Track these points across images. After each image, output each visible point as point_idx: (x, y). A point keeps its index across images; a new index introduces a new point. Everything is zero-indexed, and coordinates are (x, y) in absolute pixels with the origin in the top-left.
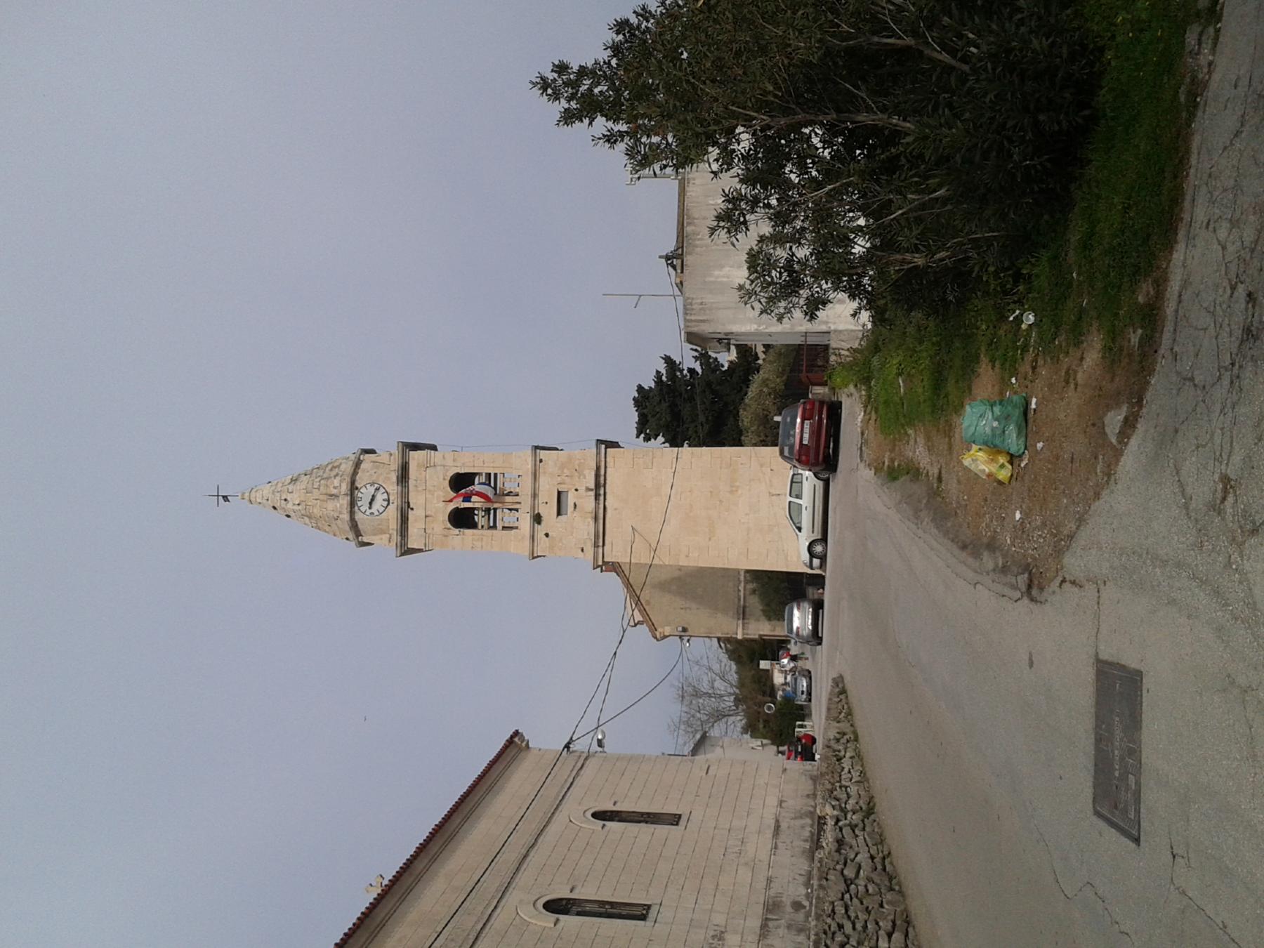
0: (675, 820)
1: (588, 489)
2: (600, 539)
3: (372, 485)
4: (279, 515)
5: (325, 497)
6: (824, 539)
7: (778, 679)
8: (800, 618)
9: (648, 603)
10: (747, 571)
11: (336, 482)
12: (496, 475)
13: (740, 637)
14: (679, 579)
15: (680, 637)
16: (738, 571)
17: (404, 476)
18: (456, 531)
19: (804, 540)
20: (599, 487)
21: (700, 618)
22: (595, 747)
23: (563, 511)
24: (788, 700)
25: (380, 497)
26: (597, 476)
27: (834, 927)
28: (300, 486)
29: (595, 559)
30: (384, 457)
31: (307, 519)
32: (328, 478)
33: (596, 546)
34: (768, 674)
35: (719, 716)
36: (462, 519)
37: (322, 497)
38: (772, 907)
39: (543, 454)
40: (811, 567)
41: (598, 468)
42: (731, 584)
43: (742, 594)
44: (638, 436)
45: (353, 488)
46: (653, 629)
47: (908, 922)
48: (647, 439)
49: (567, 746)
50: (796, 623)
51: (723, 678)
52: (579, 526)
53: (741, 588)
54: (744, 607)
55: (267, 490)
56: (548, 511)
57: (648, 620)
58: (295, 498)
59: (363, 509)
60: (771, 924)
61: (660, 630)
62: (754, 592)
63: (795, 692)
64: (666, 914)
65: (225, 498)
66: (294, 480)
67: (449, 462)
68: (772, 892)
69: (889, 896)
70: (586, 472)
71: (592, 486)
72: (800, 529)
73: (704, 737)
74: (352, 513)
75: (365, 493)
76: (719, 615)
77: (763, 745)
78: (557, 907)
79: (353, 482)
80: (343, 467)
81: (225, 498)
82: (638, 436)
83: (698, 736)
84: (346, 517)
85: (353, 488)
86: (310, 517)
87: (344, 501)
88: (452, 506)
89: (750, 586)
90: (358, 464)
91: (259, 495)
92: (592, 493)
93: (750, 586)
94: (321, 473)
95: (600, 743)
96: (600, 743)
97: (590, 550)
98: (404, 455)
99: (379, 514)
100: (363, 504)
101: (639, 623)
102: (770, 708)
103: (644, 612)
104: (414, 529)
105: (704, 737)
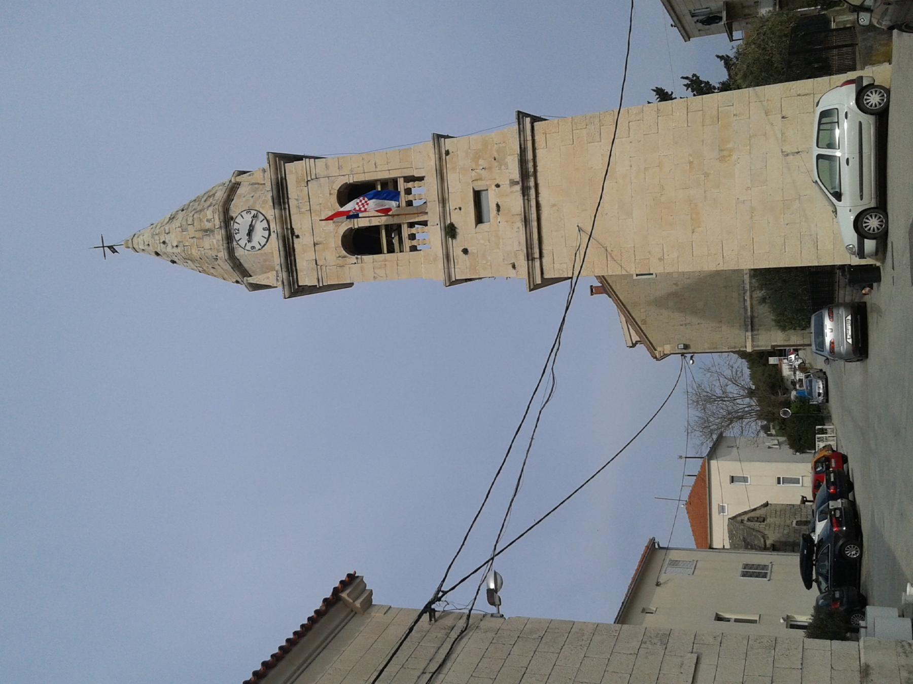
1: (513, 183)
2: (534, 250)
3: (248, 211)
4: (164, 263)
6: (881, 206)
7: (786, 371)
8: (835, 330)
9: (644, 322)
13: (749, 350)
14: (675, 294)
15: (683, 354)
16: (739, 272)
18: (353, 259)
19: (847, 218)
20: (527, 175)
21: (702, 332)
22: (483, 606)
23: (485, 218)
24: (804, 400)
25: (260, 226)
26: (523, 162)
28: (176, 223)
29: (530, 274)
30: (258, 177)
33: (530, 257)
34: (777, 368)
35: (734, 417)
36: (362, 242)
40: (861, 253)
41: (523, 151)
42: (735, 295)
43: (748, 303)
45: (227, 220)
46: (652, 348)
50: (829, 337)
51: (735, 383)
52: (504, 236)
53: (747, 297)
54: (752, 317)
55: (147, 237)
56: (464, 218)
58: (173, 239)
59: (242, 243)
61: (659, 349)
62: (763, 300)
63: (810, 393)
66: (172, 218)
67: (334, 171)
71: (516, 176)
72: (838, 196)
73: (721, 437)
75: (242, 223)
76: (724, 328)
77: (779, 444)
79: (226, 210)
83: (715, 437)
84: (223, 254)
87: (219, 235)
88: (345, 225)
89: (759, 294)
91: (140, 240)
92: (518, 188)
93: (759, 294)
95: (492, 595)
96: (492, 595)
97: (522, 263)
98: (277, 169)
99: (261, 247)
100: (241, 236)
101: (637, 342)
102: (785, 413)
103: (640, 331)
104: (303, 261)
105: (721, 437)
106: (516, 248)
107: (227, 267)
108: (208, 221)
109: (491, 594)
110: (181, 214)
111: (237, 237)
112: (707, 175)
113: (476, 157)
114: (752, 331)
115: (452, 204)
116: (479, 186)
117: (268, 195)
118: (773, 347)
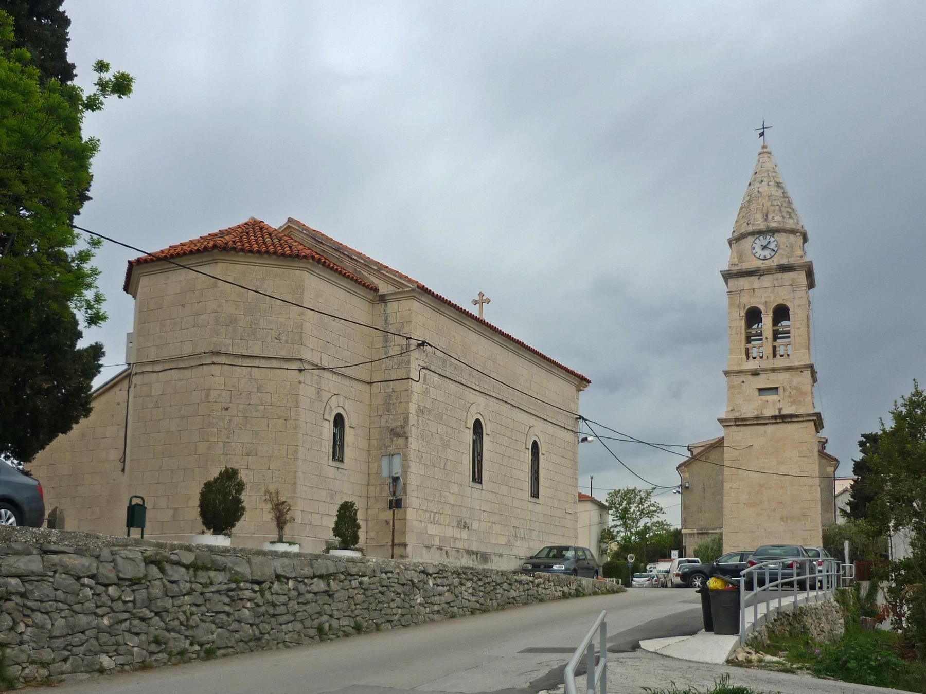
0: (535, 494)
1: (780, 410)
5: (765, 211)
10: (721, 534)
11: (778, 218)
12: (789, 337)
17: (784, 269)
18: (743, 313)
20: (783, 418)
22: (582, 436)
26: (791, 416)
27: (480, 577)
31: (748, 199)
32: (780, 211)
33: (736, 420)
36: (753, 316)
37: (765, 208)
38: (485, 557)
39: (808, 373)
41: (797, 416)
44: (863, 436)
45: (773, 231)
47: (484, 611)
48: (861, 444)
49: (581, 417)
54: (707, 533)
56: (763, 381)
57: (694, 459)
58: (764, 189)
59: (757, 241)
60: (474, 556)
64: (476, 494)
65: (762, 134)
66: (778, 185)
68: (493, 557)
69: (495, 603)
70: (794, 407)
71: (784, 412)
74: (753, 234)
75: (773, 241)
78: (478, 427)
80: (791, 221)
81: (762, 134)
82: (863, 436)
85: (773, 231)
86: (749, 201)
87: (762, 226)
88: (762, 308)
90: (793, 232)
92: (777, 413)
94: (786, 205)
99: (756, 254)
100: (762, 241)
106: (743, 411)
107: (743, 231)
108: (773, 218)
109: (586, 439)
110: (780, 192)
111: (761, 238)
112: (774, 510)
113: (797, 388)
114: (698, 533)
115: (772, 376)
116: (781, 391)
117: (784, 261)
118: (685, 547)
